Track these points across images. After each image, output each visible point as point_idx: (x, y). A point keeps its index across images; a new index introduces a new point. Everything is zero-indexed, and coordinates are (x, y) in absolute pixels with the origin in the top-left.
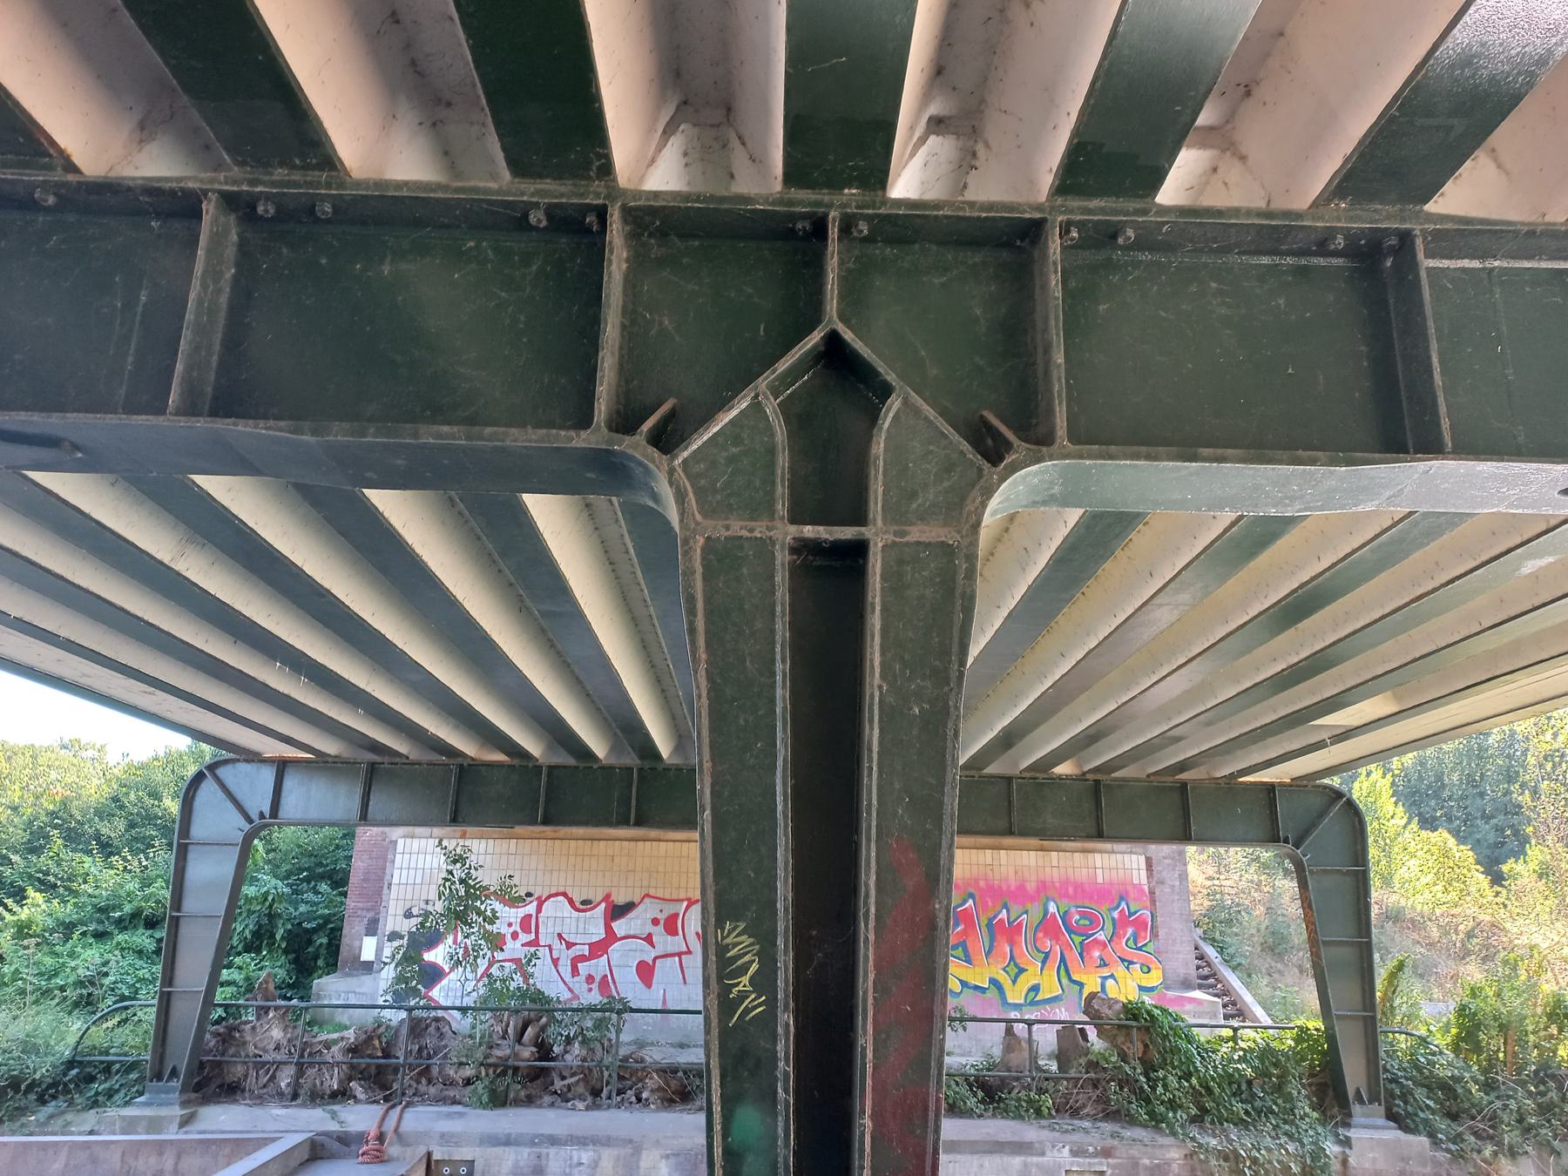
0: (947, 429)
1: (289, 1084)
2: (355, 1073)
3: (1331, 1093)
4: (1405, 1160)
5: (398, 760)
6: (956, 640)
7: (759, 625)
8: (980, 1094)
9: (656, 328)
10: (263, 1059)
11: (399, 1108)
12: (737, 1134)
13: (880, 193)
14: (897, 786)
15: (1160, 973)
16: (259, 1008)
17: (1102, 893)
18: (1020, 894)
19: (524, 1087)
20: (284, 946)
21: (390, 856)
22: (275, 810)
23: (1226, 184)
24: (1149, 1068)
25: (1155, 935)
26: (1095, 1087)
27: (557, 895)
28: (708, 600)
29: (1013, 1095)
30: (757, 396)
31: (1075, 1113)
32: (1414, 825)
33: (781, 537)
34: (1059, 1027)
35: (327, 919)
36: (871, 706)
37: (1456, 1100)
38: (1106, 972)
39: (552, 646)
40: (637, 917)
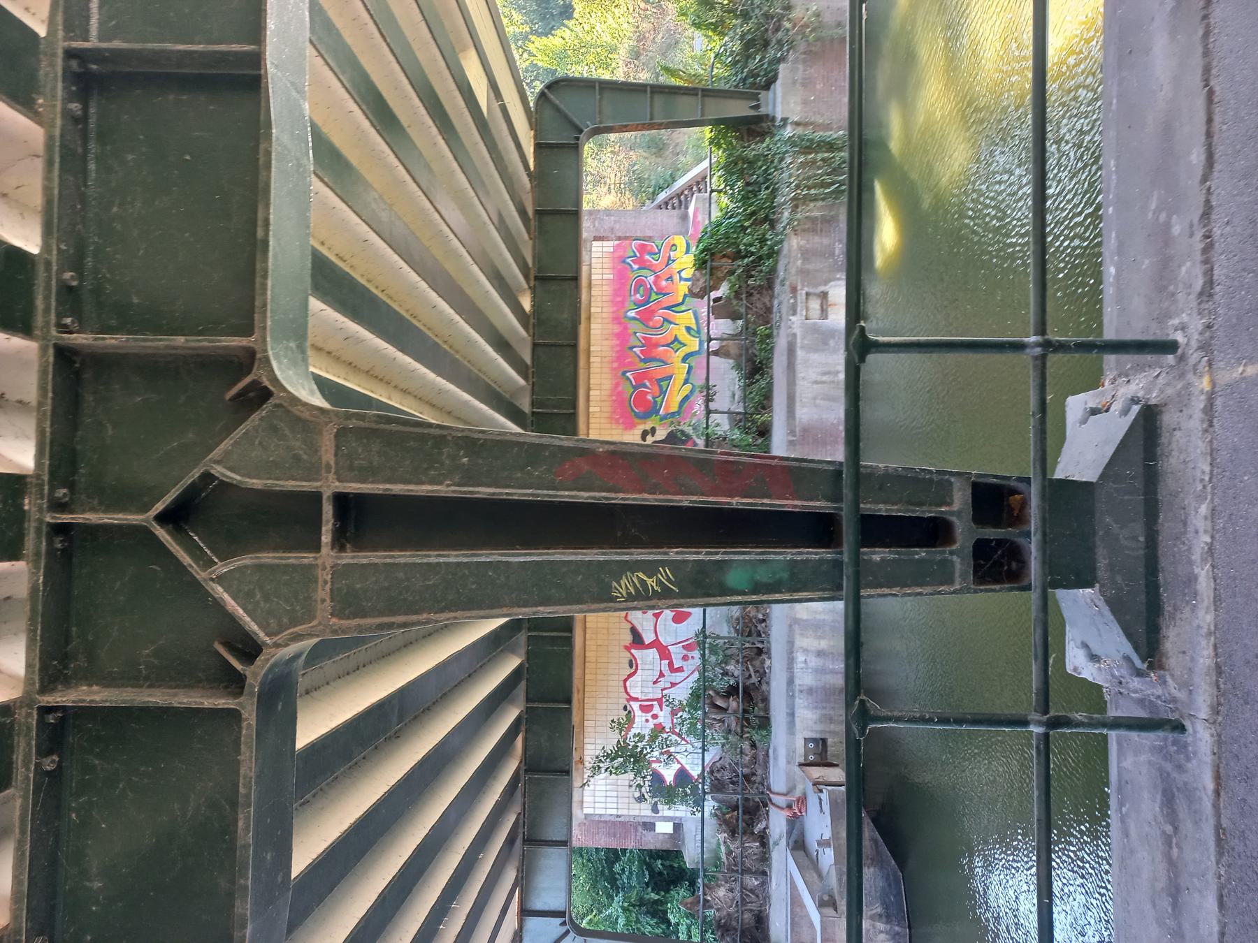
0: (241, 430)
1: (756, 879)
2: (748, 831)
3: (753, 127)
4: (794, 82)
5: (521, 822)
6: (412, 429)
7: (401, 575)
8: (757, 377)
9: (152, 659)
10: (739, 900)
11: (771, 796)
12: (745, 586)
13: (29, 480)
14: (519, 475)
15: (676, 237)
16: (704, 907)
17: (621, 276)
18: (623, 337)
19: (756, 704)
20: (663, 893)
21: (597, 818)
22: (559, 914)
23: (18, 187)
24: (738, 255)
25: (650, 239)
26: (751, 295)
27: (625, 687)
28: (381, 614)
29: (757, 353)
30: (212, 580)
31: (769, 310)
32: (570, 23)
33: (331, 560)
34: (712, 317)
35: (642, 862)
36: (461, 492)
37: (755, 40)
38: (677, 277)
39: (428, 709)
40: (642, 626)
